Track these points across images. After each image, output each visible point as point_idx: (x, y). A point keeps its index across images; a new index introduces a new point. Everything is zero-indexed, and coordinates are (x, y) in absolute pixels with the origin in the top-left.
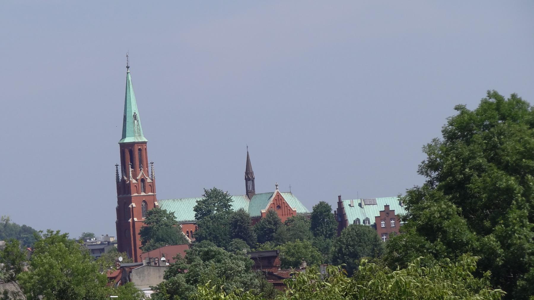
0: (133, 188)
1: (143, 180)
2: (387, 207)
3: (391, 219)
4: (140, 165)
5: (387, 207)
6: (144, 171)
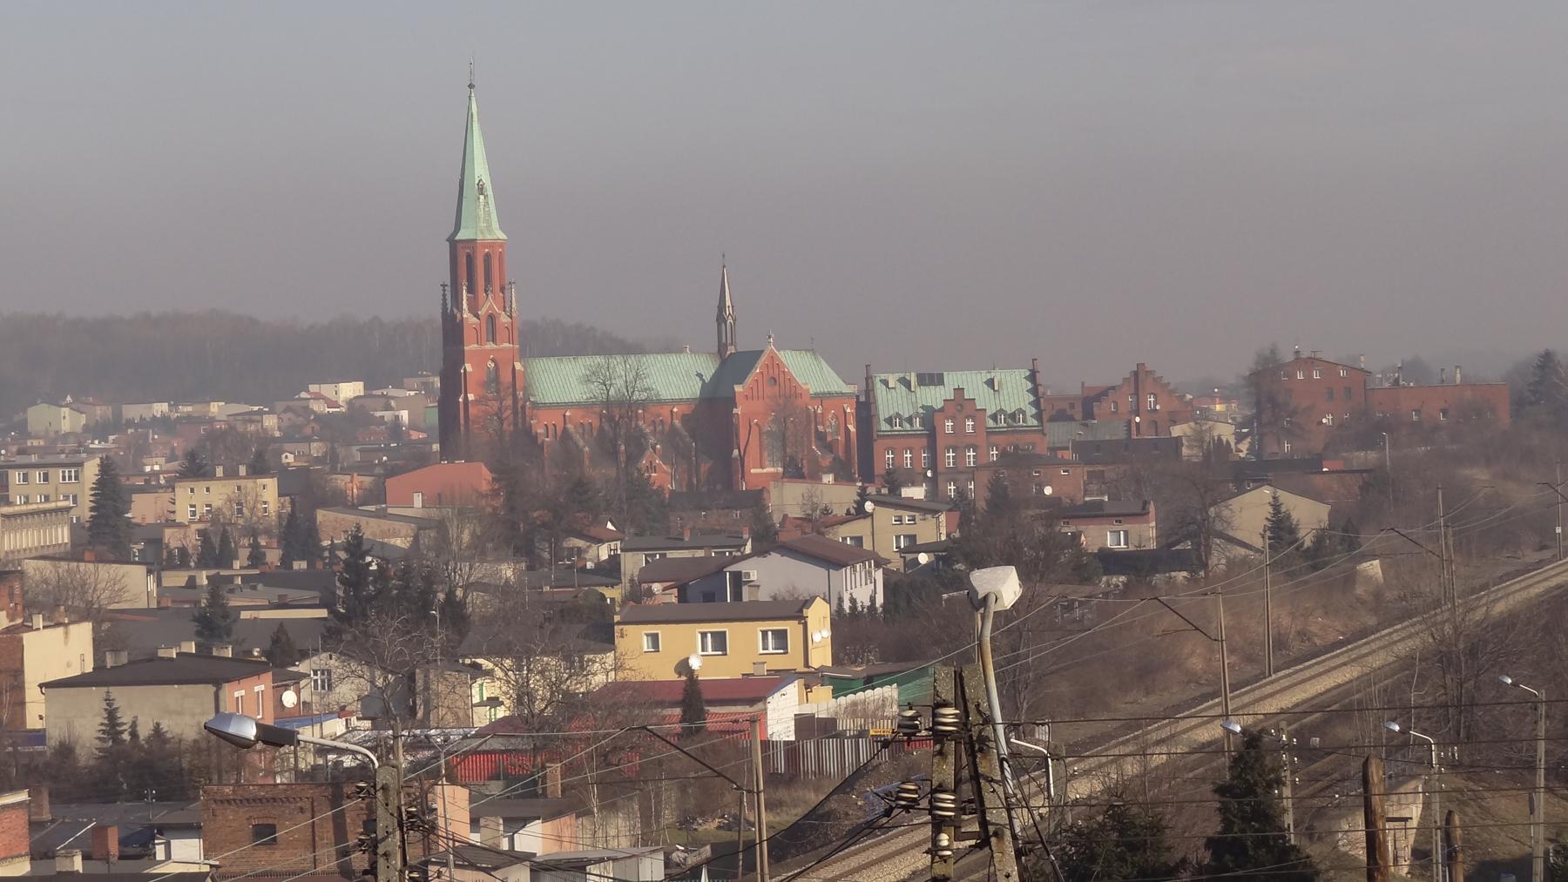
0: (468, 334)
1: (492, 318)
3: (968, 417)
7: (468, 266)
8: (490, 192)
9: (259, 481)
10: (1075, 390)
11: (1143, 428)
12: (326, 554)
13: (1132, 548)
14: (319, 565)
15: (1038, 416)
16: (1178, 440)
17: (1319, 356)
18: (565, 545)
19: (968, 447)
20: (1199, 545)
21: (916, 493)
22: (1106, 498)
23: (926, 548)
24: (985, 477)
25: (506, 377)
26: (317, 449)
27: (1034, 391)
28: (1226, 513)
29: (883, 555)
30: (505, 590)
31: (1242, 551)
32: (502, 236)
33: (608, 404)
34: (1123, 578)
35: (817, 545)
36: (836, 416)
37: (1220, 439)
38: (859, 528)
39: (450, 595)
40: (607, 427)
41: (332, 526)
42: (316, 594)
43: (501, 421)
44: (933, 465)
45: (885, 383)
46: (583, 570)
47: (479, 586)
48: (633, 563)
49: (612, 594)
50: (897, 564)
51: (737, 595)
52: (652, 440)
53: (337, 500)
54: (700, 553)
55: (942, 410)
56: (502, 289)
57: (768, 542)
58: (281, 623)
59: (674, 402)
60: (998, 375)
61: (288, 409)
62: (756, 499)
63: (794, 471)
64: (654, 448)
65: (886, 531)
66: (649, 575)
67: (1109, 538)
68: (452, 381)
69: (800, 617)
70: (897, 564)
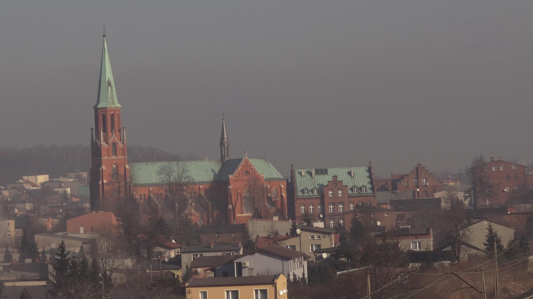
0: (104, 152)
1: (115, 144)
2: (335, 177)
3: (339, 189)
4: (112, 129)
5: (335, 177)
6: (116, 135)
7: (103, 119)
8: (113, 85)
9: (7, 222)
10: (389, 177)
11: (420, 194)
12: (41, 255)
13: (423, 250)
14: (38, 261)
15: (372, 189)
16: (439, 200)
17: (502, 159)
18: (155, 250)
19: (339, 203)
20: (455, 248)
21: (320, 225)
22: (410, 227)
23: (326, 251)
24: (349, 218)
25: (121, 172)
26: (28, 207)
27: (370, 177)
28: (467, 233)
29: (307, 254)
30: (129, 272)
31: (475, 251)
32: (119, 106)
33: (170, 184)
34: (420, 264)
35: (274, 248)
36: (276, 189)
37: (458, 199)
38: (293, 241)
39: (104, 274)
40: (169, 195)
41: (46, 243)
42: (38, 274)
43: (119, 192)
44: (323, 212)
45: (300, 173)
46: (164, 262)
47: (117, 270)
48: (187, 259)
49: (179, 273)
50: (313, 258)
51: (240, 273)
52: (190, 201)
53: (42, 230)
54: (220, 254)
55: (327, 186)
56: (119, 131)
57: (251, 248)
58: (25, 288)
59: (201, 183)
60: (353, 170)
61: (14, 188)
62: (243, 228)
63: (258, 215)
64: (191, 205)
65: (306, 243)
66: (196, 263)
67: (412, 245)
68: (96, 174)
69: (273, 284)
70: (313, 258)
